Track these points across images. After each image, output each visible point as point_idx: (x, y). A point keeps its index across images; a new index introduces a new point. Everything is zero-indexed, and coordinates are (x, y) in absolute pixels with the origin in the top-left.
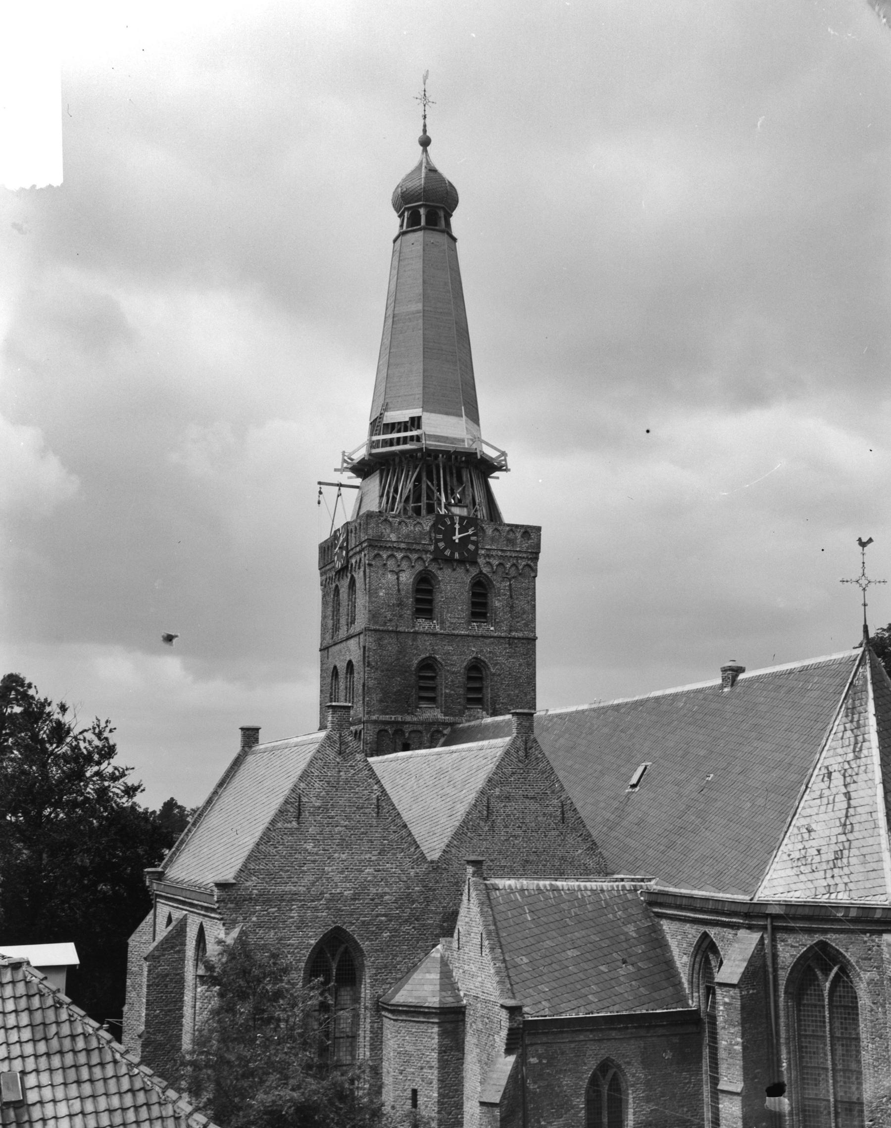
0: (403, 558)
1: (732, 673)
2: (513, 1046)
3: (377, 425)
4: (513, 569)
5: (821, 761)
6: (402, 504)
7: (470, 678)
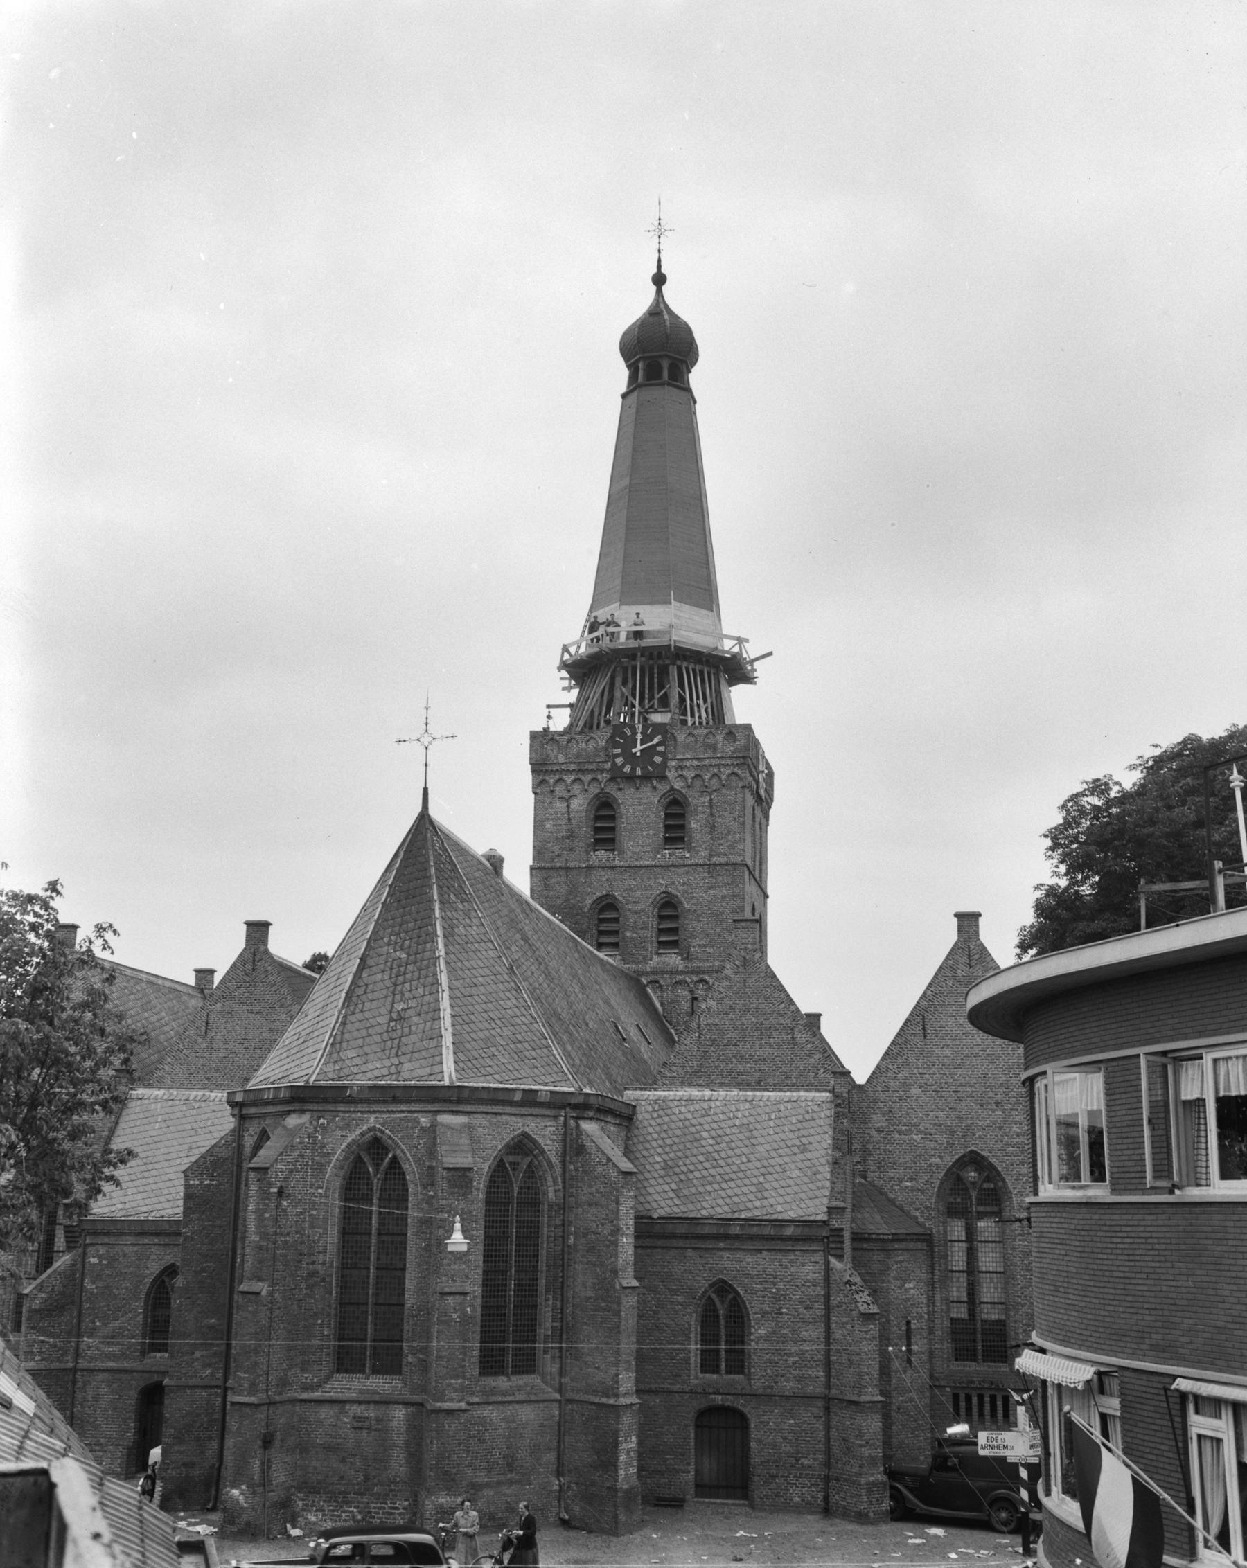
0: (574, 781)
2: (72, 1245)
7: (661, 918)
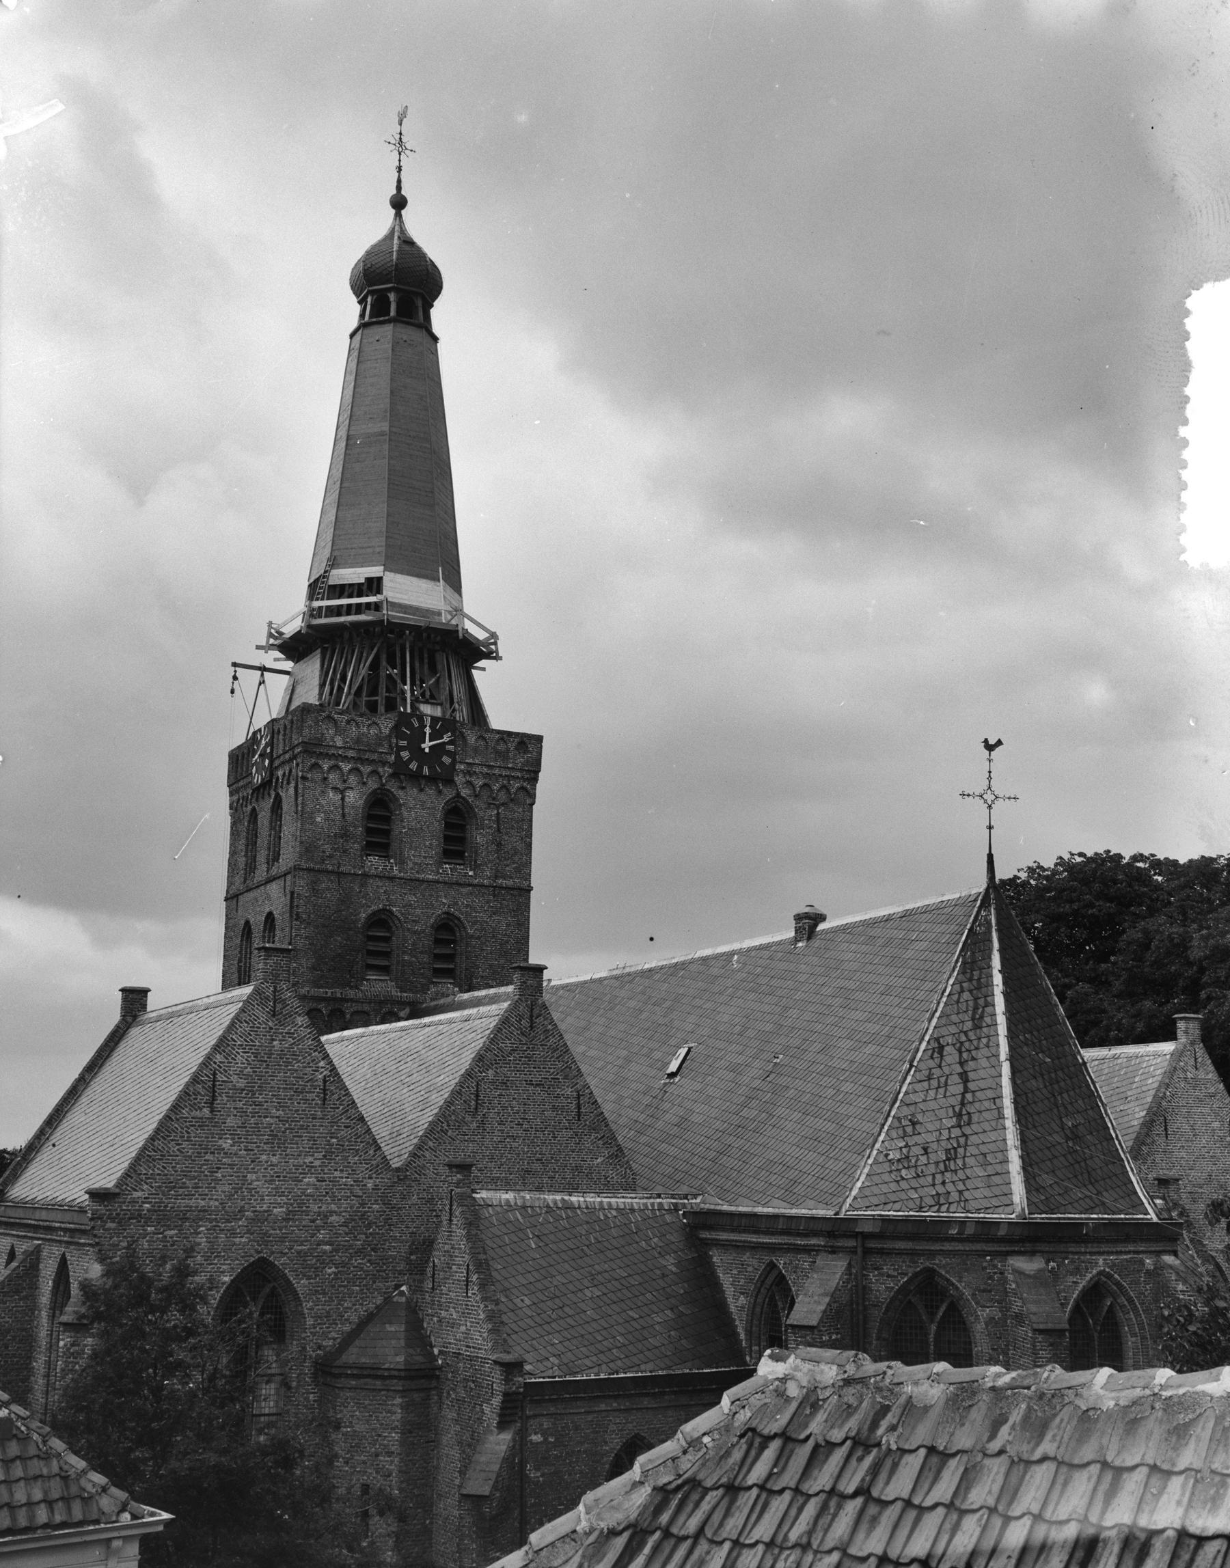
0: (350, 771)
1: (808, 923)
2: (508, 1419)
3: (315, 589)
4: (503, 792)
5: (930, 1032)
6: (351, 697)
7: (438, 942)
